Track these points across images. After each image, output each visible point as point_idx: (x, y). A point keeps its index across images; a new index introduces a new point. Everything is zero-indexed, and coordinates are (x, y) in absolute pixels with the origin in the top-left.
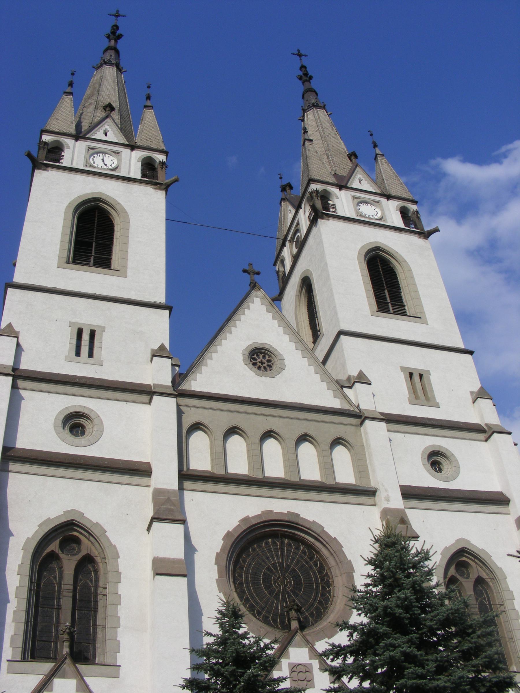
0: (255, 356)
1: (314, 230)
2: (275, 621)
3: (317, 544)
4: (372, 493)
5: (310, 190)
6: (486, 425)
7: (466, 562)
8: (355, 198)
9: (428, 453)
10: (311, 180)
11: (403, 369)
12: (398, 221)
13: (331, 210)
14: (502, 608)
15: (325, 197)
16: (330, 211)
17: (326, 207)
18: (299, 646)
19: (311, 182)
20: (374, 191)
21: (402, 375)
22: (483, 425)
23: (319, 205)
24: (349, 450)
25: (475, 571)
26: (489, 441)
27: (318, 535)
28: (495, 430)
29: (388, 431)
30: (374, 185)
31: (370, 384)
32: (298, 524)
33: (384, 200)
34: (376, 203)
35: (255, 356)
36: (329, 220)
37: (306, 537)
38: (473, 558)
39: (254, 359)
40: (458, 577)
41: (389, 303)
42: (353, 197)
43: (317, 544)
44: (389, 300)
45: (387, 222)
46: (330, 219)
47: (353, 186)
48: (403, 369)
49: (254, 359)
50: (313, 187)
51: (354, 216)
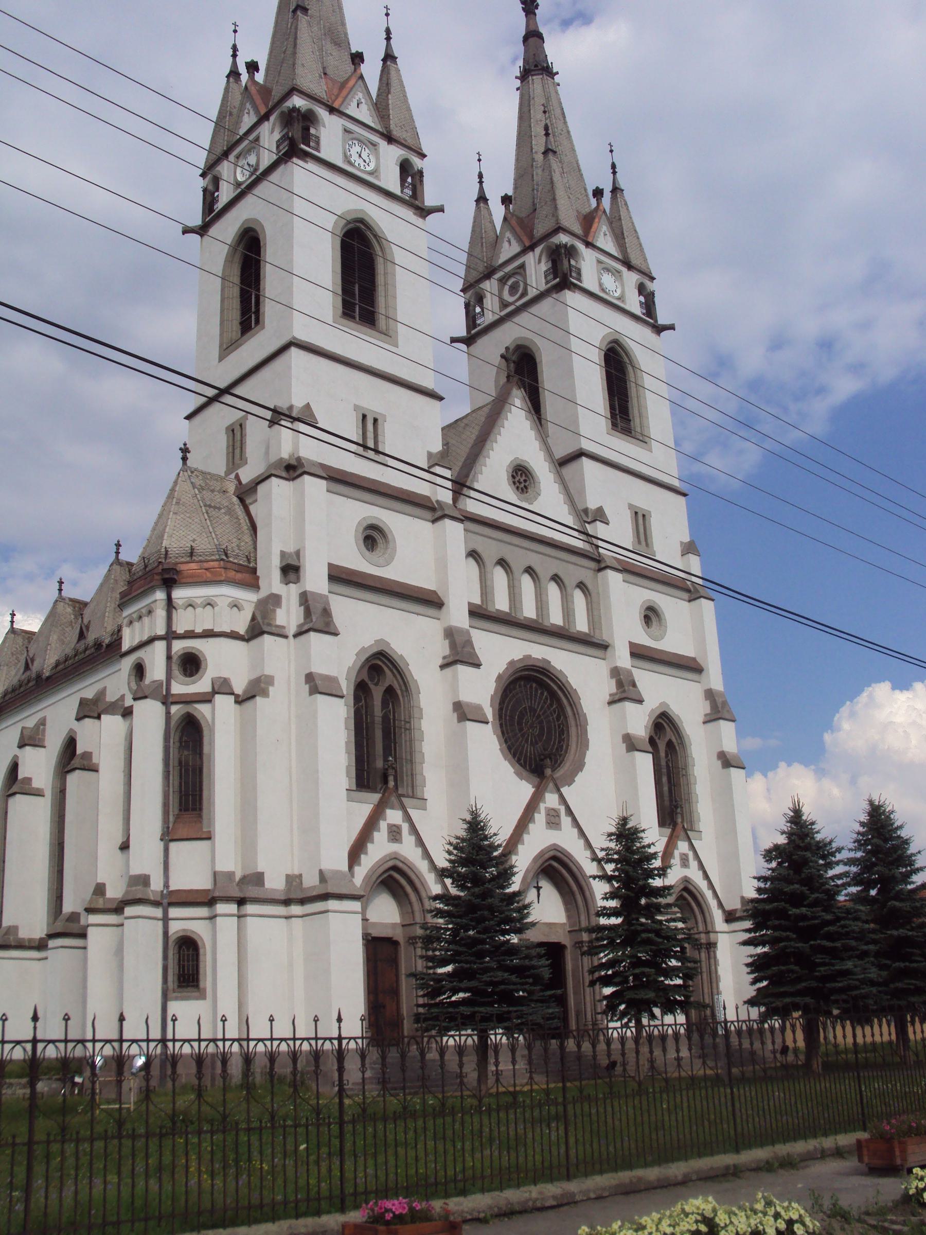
0: (519, 473)
1: (281, 169)
2: (525, 762)
3: (559, 693)
4: (604, 647)
5: (289, 104)
6: (437, 501)
7: (381, 666)
8: (347, 131)
9: (370, 523)
10: (294, 90)
11: (631, 506)
12: (391, 180)
13: (312, 144)
14: (408, 726)
15: (308, 118)
16: (309, 146)
17: (306, 138)
18: (551, 792)
19: (295, 93)
20: (372, 125)
21: (628, 512)
22: (434, 500)
23: (296, 132)
24: (507, 573)
25: (389, 679)
26: (693, 603)
27: (563, 685)
28: (609, 564)
29: (624, 581)
30: (375, 116)
31: (607, 524)
32: (548, 671)
33: (383, 144)
34: (370, 146)
35: (519, 473)
36: (574, 292)
37: (552, 684)
38: (391, 666)
39: (517, 473)
40: (369, 683)
41: (356, 304)
42: (345, 130)
43: (559, 693)
44: (617, 412)
45: (625, 304)
46: (576, 291)
47: (348, 112)
48: (631, 506)
49: (517, 473)
50: (297, 101)
51: (340, 163)
